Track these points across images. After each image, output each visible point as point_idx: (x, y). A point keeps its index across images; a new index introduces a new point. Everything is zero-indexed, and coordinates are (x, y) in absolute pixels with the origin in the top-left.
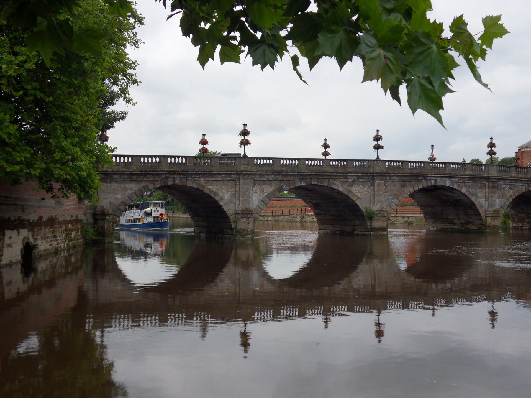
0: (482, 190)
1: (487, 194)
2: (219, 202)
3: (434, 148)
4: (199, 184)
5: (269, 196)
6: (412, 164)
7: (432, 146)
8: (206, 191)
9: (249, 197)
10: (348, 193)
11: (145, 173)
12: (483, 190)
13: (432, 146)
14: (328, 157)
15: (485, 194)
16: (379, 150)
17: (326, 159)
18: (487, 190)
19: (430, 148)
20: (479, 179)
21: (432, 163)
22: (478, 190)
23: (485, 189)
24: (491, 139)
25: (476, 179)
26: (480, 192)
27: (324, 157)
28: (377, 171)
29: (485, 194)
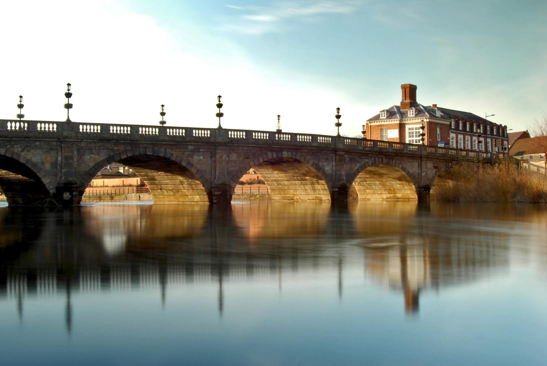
0: (329, 164)
1: (334, 168)
2: (37, 174)
3: (281, 118)
4: (13, 153)
5: (96, 168)
6: (174, 130)
7: (279, 116)
8: (22, 160)
9: (347, 155)
10: (186, 166)
11: (130, 142)
12: (330, 163)
13: (279, 116)
14: (164, 125)
15: (332, 167)
16: (67, 103)
17: (163, 127)
18: (334, 163)
19: (277, 118)
20: (326, 152)
21: (20, 122)
22: (325, 164)
23: (332, 162)
24: (338, 109)
25: (323, 152)
26: (327, 165)
27: (19, 119)
28: (218, 141)
29: (332, 167)
